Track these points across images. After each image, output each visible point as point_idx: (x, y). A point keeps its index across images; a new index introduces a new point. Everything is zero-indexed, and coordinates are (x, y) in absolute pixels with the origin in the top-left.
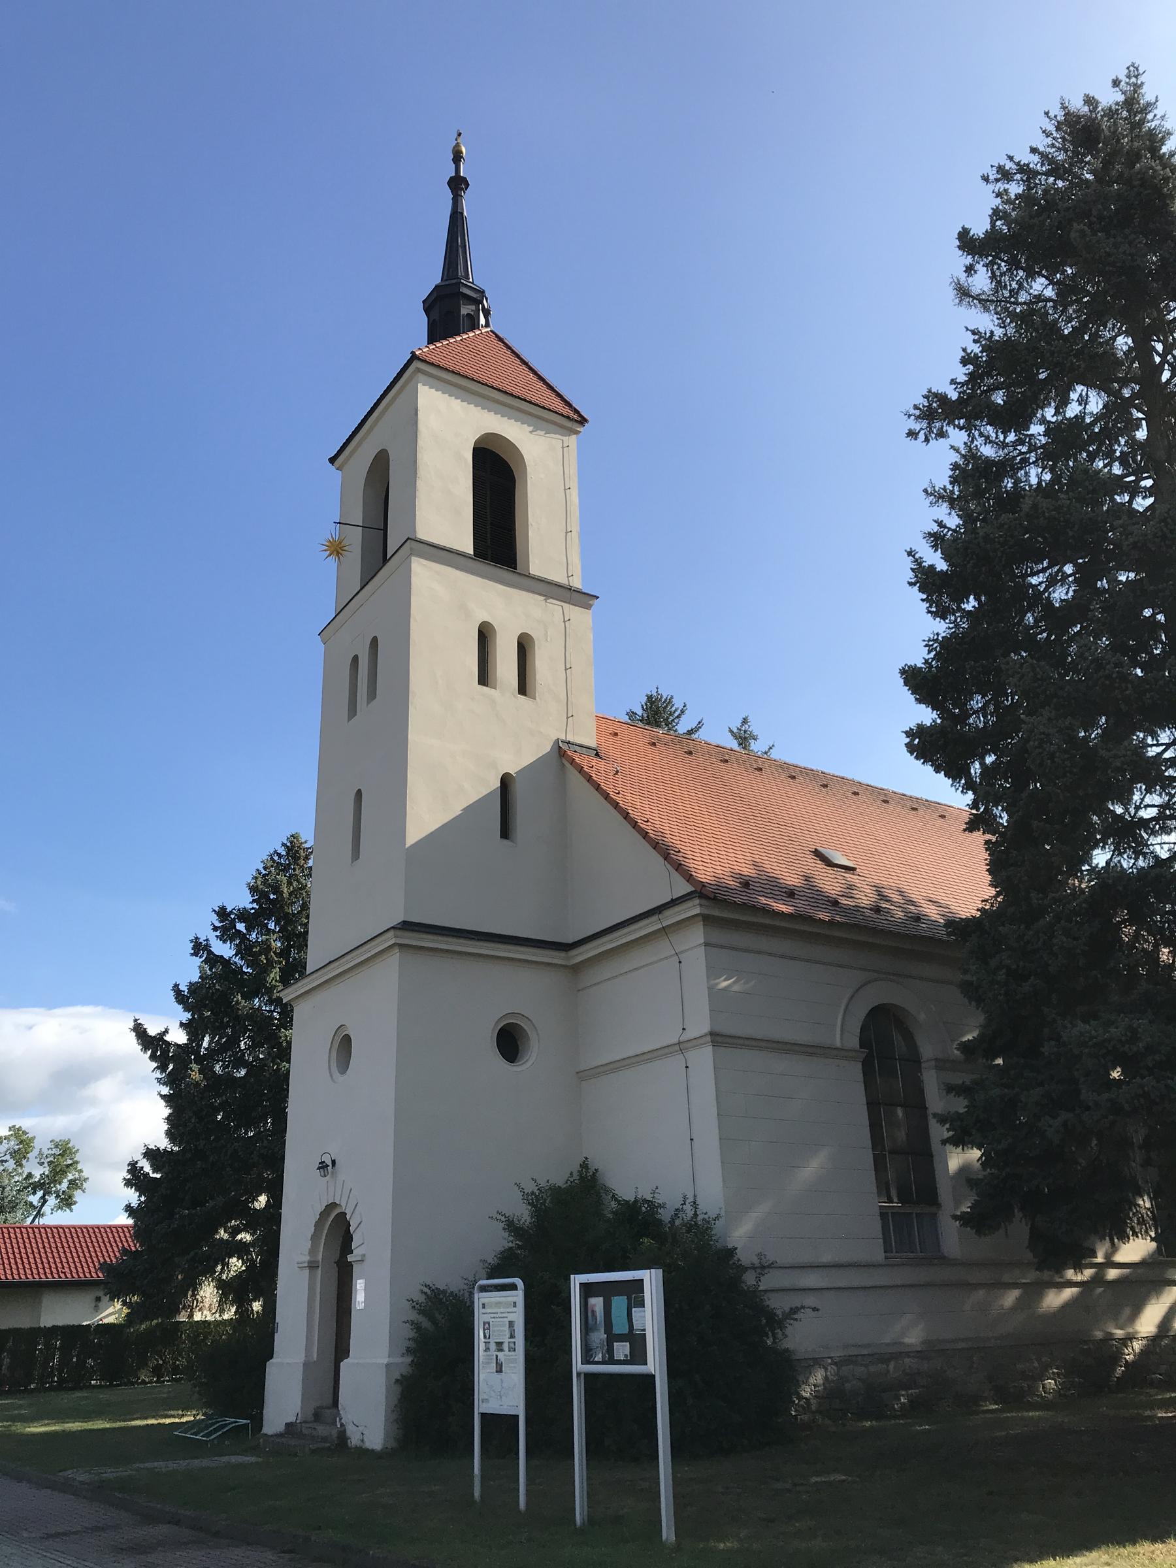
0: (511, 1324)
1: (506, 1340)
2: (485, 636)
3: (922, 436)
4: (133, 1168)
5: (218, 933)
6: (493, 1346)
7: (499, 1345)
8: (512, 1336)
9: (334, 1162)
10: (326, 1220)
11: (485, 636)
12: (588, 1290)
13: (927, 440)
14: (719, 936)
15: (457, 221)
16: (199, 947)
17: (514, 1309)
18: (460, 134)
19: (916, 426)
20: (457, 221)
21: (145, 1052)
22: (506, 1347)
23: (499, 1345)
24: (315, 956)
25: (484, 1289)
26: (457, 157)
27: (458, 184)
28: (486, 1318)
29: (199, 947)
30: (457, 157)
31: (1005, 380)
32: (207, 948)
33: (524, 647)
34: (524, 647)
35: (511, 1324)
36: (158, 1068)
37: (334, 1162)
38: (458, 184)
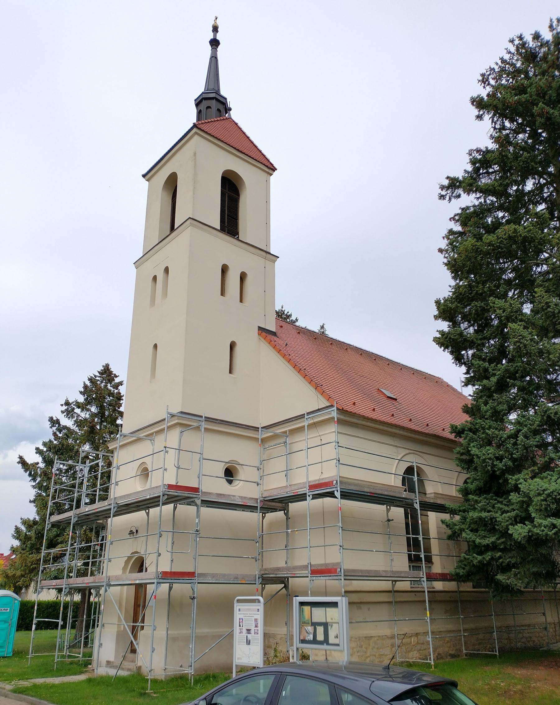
0: (256, 620)
1: (253, 628)
2: (224, 270)
3: (447, 198)
4: (17, 530)
5: (65, 414)
6: (245, 631)
7: (249, 631)
8: (256, 626)
9: (137, 531)
10: (129, 564)
11: (224, 270)
12: (302, 604)
13: (450, 199)
14: (344, 429)
15: (214, 59)
16: (54, 422)
17: (258, 613)
18: (216, 19)
19: (443, 193)
20: (214, 59)
21: (26, 472)
22: (252, 632)
23: (249, 631)
24: (128, 423)
25: (239, 601)
26: (215, 29)
27: (215, 43)
28: (241, 616)
29: (54, 422)
30: (215, 29)
31: (493, 171)
32: (58, 421)
33: (243, 277)
34: (243, 277)
35: (256, 620)
36: (32, 479)
37: (137, 531)
38: (215, 43)
